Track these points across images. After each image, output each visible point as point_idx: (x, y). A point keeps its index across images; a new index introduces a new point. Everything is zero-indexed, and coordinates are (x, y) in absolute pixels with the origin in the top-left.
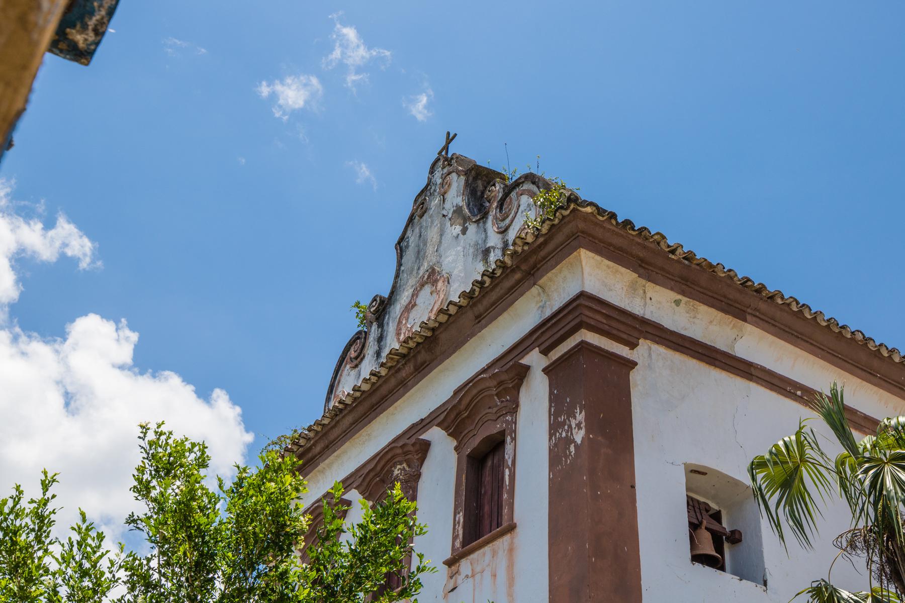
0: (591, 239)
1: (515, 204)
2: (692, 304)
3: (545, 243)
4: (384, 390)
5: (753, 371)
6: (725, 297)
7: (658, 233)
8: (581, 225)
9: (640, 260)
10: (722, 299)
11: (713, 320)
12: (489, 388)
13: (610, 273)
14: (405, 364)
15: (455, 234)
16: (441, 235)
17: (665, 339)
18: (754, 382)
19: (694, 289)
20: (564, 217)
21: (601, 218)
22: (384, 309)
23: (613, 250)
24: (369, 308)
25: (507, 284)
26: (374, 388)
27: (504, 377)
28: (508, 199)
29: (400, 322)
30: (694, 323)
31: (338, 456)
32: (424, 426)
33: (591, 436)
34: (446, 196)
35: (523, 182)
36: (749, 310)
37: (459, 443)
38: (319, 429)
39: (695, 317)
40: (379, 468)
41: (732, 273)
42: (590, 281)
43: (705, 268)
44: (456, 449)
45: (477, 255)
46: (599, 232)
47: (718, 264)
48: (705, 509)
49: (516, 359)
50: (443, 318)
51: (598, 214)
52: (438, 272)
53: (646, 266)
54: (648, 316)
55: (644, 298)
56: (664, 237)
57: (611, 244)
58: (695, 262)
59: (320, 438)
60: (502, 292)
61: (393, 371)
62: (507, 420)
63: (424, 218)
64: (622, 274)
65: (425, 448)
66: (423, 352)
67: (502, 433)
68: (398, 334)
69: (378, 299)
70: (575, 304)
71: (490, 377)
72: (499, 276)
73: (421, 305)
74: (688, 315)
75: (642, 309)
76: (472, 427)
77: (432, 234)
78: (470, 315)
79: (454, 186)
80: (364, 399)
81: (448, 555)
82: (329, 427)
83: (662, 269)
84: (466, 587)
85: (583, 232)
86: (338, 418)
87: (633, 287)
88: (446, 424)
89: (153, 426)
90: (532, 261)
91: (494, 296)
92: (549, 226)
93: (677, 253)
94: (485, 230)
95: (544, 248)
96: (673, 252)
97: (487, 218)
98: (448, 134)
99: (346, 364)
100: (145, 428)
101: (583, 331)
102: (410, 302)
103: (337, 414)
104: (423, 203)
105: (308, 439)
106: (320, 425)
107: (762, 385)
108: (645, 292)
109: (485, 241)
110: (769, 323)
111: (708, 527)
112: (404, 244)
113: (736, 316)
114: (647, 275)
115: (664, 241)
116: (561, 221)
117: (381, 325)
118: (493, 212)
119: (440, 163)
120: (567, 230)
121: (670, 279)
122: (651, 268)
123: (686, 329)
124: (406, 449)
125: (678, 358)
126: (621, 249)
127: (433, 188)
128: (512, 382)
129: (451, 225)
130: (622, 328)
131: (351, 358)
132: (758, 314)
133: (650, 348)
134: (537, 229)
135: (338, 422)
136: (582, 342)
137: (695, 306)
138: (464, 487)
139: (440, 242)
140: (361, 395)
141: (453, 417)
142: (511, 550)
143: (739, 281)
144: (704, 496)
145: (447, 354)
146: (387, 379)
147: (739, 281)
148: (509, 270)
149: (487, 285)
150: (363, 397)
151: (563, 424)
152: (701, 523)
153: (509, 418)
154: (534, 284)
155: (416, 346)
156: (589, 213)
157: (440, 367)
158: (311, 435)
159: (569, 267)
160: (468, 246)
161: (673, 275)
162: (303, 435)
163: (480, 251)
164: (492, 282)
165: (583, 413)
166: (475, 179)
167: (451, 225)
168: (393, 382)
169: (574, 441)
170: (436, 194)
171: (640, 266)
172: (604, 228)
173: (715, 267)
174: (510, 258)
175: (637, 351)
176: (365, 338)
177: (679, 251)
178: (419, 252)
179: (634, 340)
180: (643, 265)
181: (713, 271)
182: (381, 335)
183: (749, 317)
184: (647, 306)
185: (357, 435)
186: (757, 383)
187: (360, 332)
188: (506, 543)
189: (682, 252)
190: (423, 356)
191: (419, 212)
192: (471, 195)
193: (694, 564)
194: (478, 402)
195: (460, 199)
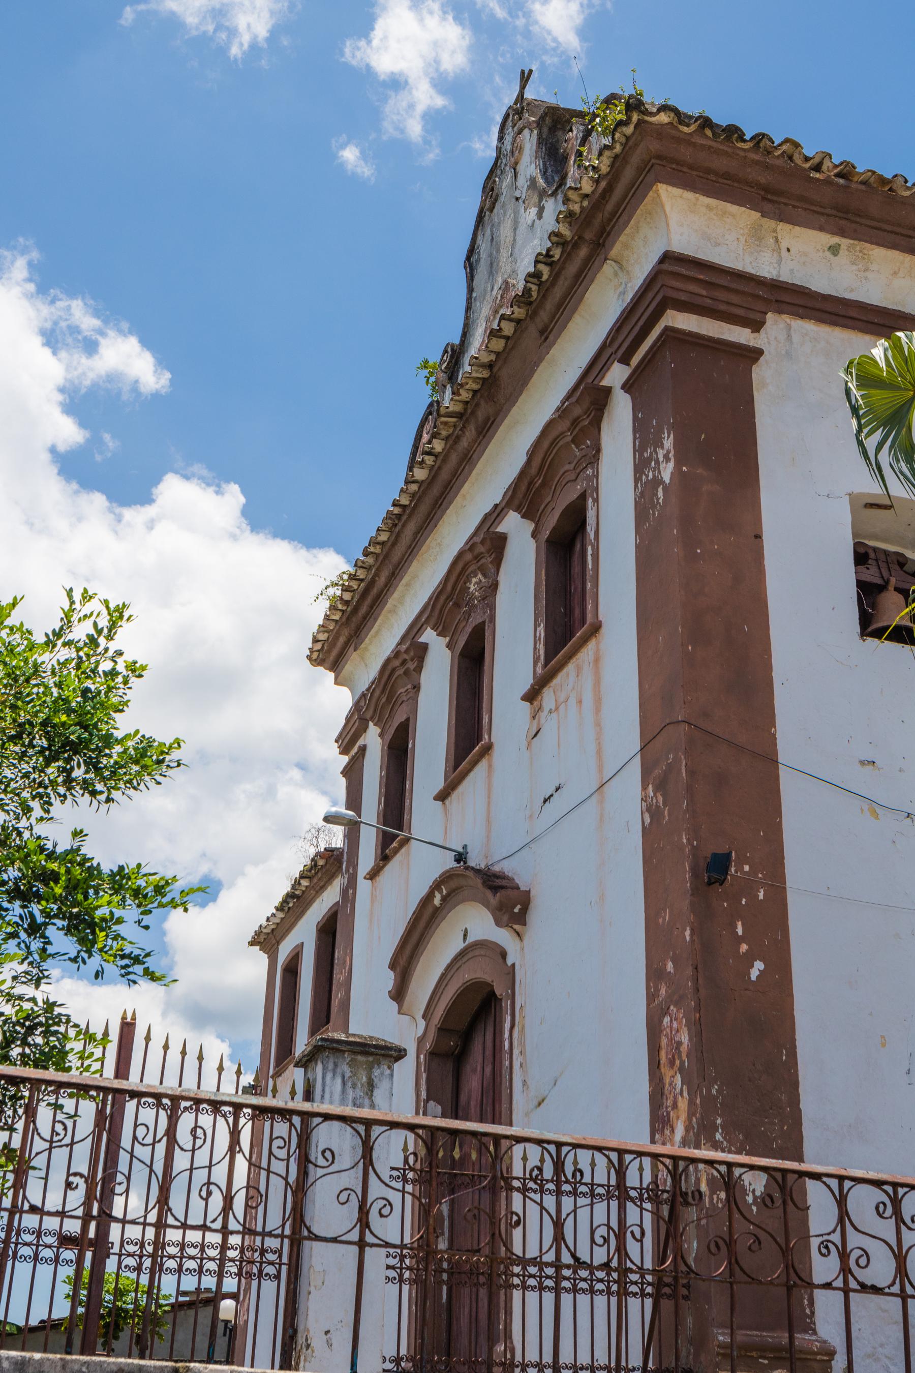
2: (858, 248)
3: (609, 189)
4: (444, 475)
7: (787, 141)
8: (654, 146)
9: (763, 190)
11: (899, 270)
13: (715, 217)
14: (464, 427)
15: (530, 222)
17: (814, 309)
19: (861, 224)
20: (628, 138)
21: (685, 129)
23: (714, 179)
24: (440, 365)
25: (572, 269)
26: (432, 474)
31: (408, 585)
32: (498, 515)
33: (684, 468)
34: (518, 168)
38: (378, 550)
39: (866, 270)
40: (449, 588)
42: (681, 235)
43: (875, 185)
44: (534, 535)
46: (686, 153)
47: (896, 176)
48: (898, 561)
50: (498, 345)
51: (680, 123)
53: (775, 198)
56: (797, 145)
57: (708, 171)
58: (855, 179)
59: (381, 564)
60: (567, 283)
61: (450, 442)
62: (588, 475)
63: (495, 210)
64: (733, 216)
67: (583, 497)
69: (449, 349)
72: (559, 260)
74: (854, 267)
75: (775, 268)
76: (549, 499)
78: (532, 331)
82: (389, 544)
83: (802, 199)
84: (549, 724)
85: (659, 157)
86: (397, 530)
87: (756, 234)
90: (597, 222)
91: (558, 292)
92: (612, 159)
93: (824, 168)
95: (610, 196)
96: (818, 168)
98: (523, 72)
104: (492, 189)
105: (369, 569)
108: (777, 241)
111: (901, 587)
112: (474, 258)
114: (777, 211)
115: (797, 151)
116: (624, 145)
120: (635, 160)
121: (818, 213)
122: (783, 200)
123: (852, 291)
126: (727, 175)
127: (504, 161)
128: (588, 416)
129: (525, 210)
130: (735, 299)
133: (789, 327)
135: (398, 535)
137: (866, 252)
138: (544, 587)
139: (515, 240)
140: (419, 488)
141: (523, 488)
142: (597, 660)
144: (899, 545)
145: (512, 399)
148: (570, 247)
149: (545, 277)
151: (650, 459)
152: (887, 582)
153: (589, 472)
154: (606, 259)
155: (473, 396)
156: (667, 124)
157: (506, 422)
158: (370, 560)
159: (648, 220)
161: (821, 207)
164: (551, 272)
165: (672, 436)
167: (525, 210)
168: (454, 459)
169: (662, 482)
170: (507, 169)
171: (764, 199)
172: (694, 145)
174: (567, 225)
175: (766, 334)
177: (827, 164)
179: (758, 317)
180: (769, 197)
184: (783, 262)
188: (591, 653)
189: (830, 165)
192: (549, 155)
193: (864, 640)
194: (552, 459)
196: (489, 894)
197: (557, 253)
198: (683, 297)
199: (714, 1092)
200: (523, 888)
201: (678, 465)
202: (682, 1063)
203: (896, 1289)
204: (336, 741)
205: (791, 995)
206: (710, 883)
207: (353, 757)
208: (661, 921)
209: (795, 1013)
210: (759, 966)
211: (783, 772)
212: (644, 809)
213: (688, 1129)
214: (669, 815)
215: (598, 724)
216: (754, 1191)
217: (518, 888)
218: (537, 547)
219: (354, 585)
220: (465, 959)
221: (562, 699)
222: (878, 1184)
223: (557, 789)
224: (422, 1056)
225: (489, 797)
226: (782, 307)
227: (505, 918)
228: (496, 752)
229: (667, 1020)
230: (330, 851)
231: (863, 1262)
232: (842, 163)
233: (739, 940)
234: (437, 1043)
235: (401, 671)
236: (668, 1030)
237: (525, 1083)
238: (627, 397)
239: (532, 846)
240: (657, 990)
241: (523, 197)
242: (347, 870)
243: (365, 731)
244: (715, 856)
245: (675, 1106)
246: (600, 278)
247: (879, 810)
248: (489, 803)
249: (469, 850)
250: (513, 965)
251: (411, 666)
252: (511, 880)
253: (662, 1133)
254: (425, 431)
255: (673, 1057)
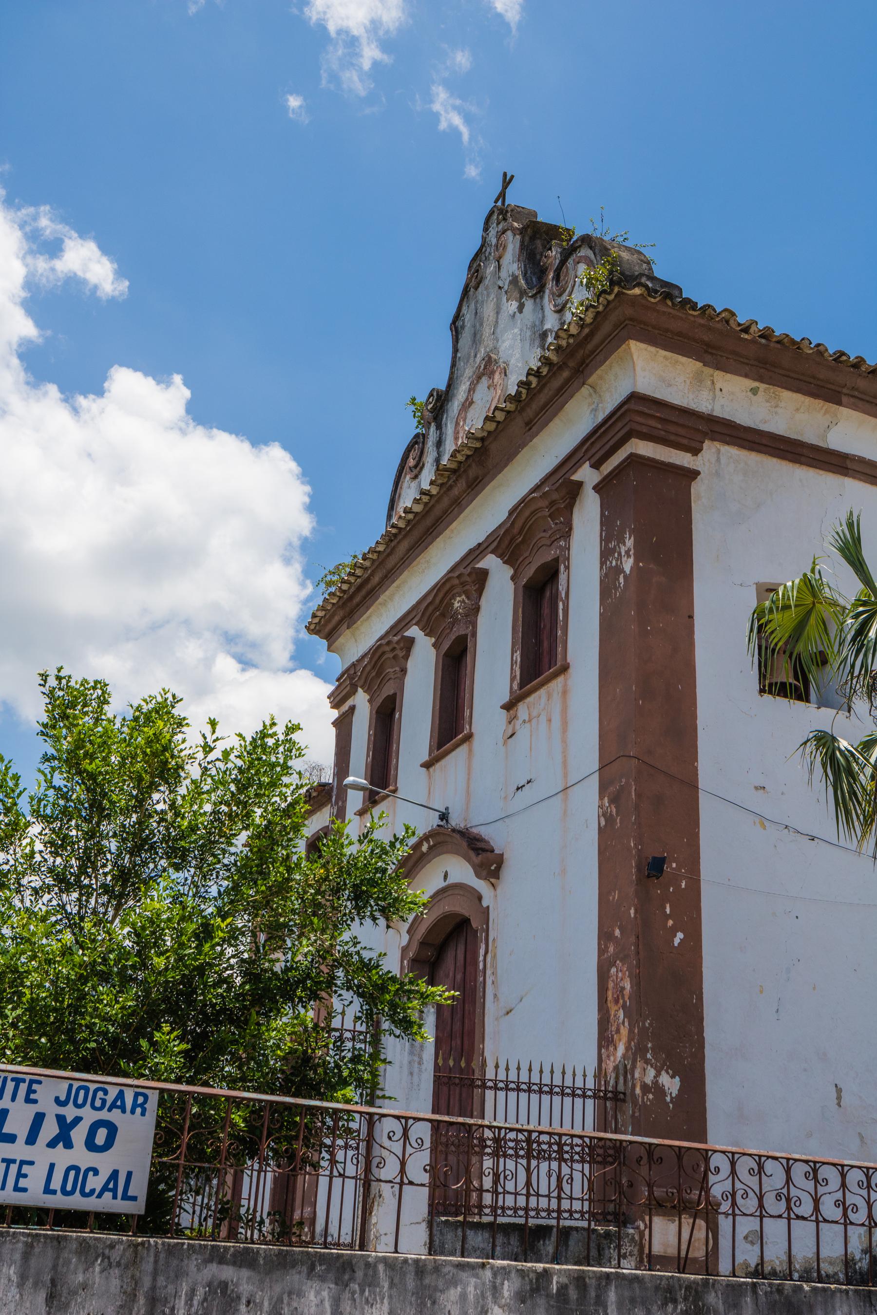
0: (642, 326)
1: (572, 273)
4: (437, 511)
5: (849, 464)
6: (814, 377)
7: (726, 310)
8: (629, 312)
10: (812, 380)
12: (540, 509)
15: (511, 312)
16: (498, 313)
18: (849, 477)
20: (609, 302)
21: (652, 300)
22: (442, 407)
24: (427, 404)
25: (556, 383)
26: (427, 509)
27: (555, 496)
28: (564, 268)
29: (457, 424)
30: (776, 413)
31: (398, 587)
32: (481, 552)
34: (501, 261)
35: (580, 246)
36: (845, 391)
37: (516, 571)
38: (375, 556)
39: (776, 406)
40: (437, 601)
41: (821, 348)
44: (513, 578)
45: (534, 340)
47: (803, 339)
49: (566, 476)
50: (491, 426)
52: (495, 360)
53: (714, 351)
54: (718, 413)
55: (713, 388)
56: (733, 314)
57: (667, 330)
58: (774, 340)
62: (561, 546)
63: (480, 289)
64: (683, 364)
65: (483, 576)
66: (474, 465)
67: (556, 560)
68: (456, 439)
69: (435, 394)
70: (623, 410)
71: (541, 497)
73: (479, 402)
74: (768, 404)
76: (527, 554)
77: (488, 311)
78: (519, 422)
79: (510, 247)
80: (418, 522)
81: (506, 698)
82: (385, 554)
84: (523, 732)
85: (631, 319)
86: (393, 544)
87: (698, 379)
88: (500, 551)
89: (52, 672)
90: (580, 354)
91: (542, 398)
93: (752, 331)
94: (542, 309)
95: (591, 340)
96: (746, 330)
97: (544, 292)
98: (505, 174)
99: (406, 474)
100: (44, 677)
101: (634, 441)
102: (467, 399)
103: (392, 538)
104: (477, 271)
105: (365, 569)
106: (376, 552)
107: (861, 480)
108: (713, 383)
109: (542, 322)
110: (872, 403)
112: (459, 323)
113: (828, 399)
116: (606, 307)
117: (439, 427)
118: (550, 285)
119: (495, 217)
120: (613, 318)
121: (744, 363)
124: (463, 579)
125: (753, 458)
127: (488, 250)
131: (410, 468)
132: (856, 393)
133: (719, 451)
134: (581, 318)
135: (394, 548)
136: (632, 455)
138: (520, 622)
139: (497, 322)
141: (506, 542)
142: (565, 693)
143: (831, 356)
146: (439, 498)
147: (831, 356)
148: (555, 368)
149: (533, 386)
150: (417, 518)
151: (613, 551)
153: (562, 543)
154: (584, 384)
158: (367, 563)
160: (525, 329)
162: (358, 565)
163: (537, 335)
165: (632, 538)
166: (533, 238)
168: (446, 501)
170: (491, 258)
171: (706, 352)
172: (658, 311)
173: (798, 343)
176: (423, 443)
177: (753, 329)
178: (475, 334)
181: (798, 348)
182: (440, 438)
183: (845, 399)
185: (415, 563)
186: (854, 478)
187: (417, 436)
188: (560, 685)
190: (473, 472)
191: (473, 283)
195: (515, 266)
196: (472, 854)
197: (545, 371)
198: (645, 430)
199: (647, 1025)
200: (497, 852)
201: (636, 561)
202: (625, 1002)
203: (813, 1218)
204: (329, 697)
205: (701, 957)
206: (649, 876)
207: (344, 714)
208: (611, 898)
209: (704, 969)
210: (680, 935)
211: (701, 794)
212: (601, 814)
213: (628, 1048)
214: (620, 823)
215: (564, 741)
216: (671, 1094)
217: (493, 851)
218: (515, 589)
219: (352, 579)
220: (445, 895)
221: (534, 714)
222: (806, 1162)
223: (528, 782)
224: (405, 962)
225: (469, 774)
226: (715, 436)
227: (484, 873)
228: (476, 740)
229: (613, 970)
230: (322, 786)
231: (798, 1203)
232: (765, 328)
233: (668, 917)
234: (418, 953)
235: (391, 655)
236: (615, 977)
237: (495, 996)
238: (597, 496)
239: (505, 820)
240: (607, 947)
241: (506, 287)
242: (337, 803)
243: (354, 694)
244: (654, 858)
245: (618, 1031)
246: (578, 396)
247: (766, 823)
248: (469, 779)
249: (450, 811)
250: (488, 907)
251: (401, 654)
252: (487, 842)
253: (607, 1049)
254: (411, 457)
255: (618, 996)
